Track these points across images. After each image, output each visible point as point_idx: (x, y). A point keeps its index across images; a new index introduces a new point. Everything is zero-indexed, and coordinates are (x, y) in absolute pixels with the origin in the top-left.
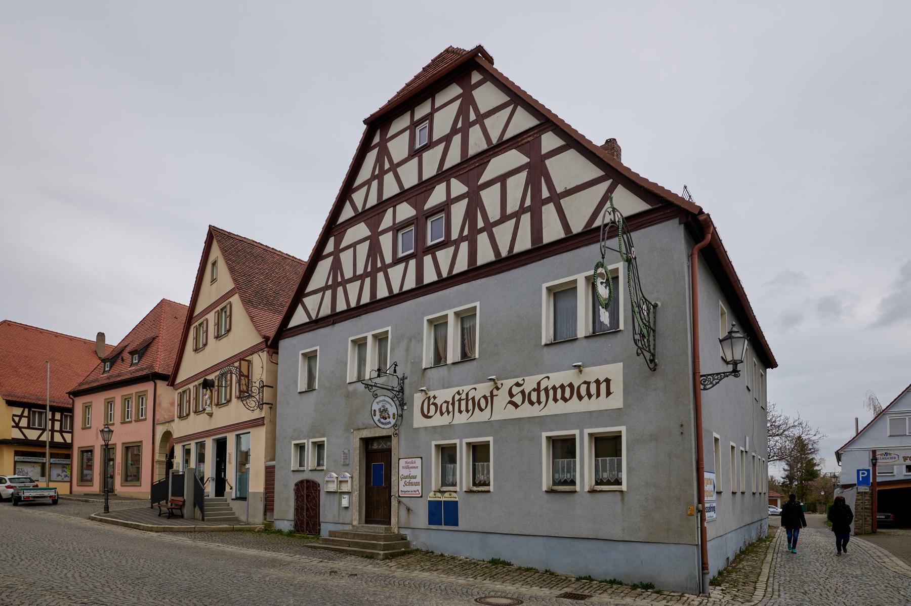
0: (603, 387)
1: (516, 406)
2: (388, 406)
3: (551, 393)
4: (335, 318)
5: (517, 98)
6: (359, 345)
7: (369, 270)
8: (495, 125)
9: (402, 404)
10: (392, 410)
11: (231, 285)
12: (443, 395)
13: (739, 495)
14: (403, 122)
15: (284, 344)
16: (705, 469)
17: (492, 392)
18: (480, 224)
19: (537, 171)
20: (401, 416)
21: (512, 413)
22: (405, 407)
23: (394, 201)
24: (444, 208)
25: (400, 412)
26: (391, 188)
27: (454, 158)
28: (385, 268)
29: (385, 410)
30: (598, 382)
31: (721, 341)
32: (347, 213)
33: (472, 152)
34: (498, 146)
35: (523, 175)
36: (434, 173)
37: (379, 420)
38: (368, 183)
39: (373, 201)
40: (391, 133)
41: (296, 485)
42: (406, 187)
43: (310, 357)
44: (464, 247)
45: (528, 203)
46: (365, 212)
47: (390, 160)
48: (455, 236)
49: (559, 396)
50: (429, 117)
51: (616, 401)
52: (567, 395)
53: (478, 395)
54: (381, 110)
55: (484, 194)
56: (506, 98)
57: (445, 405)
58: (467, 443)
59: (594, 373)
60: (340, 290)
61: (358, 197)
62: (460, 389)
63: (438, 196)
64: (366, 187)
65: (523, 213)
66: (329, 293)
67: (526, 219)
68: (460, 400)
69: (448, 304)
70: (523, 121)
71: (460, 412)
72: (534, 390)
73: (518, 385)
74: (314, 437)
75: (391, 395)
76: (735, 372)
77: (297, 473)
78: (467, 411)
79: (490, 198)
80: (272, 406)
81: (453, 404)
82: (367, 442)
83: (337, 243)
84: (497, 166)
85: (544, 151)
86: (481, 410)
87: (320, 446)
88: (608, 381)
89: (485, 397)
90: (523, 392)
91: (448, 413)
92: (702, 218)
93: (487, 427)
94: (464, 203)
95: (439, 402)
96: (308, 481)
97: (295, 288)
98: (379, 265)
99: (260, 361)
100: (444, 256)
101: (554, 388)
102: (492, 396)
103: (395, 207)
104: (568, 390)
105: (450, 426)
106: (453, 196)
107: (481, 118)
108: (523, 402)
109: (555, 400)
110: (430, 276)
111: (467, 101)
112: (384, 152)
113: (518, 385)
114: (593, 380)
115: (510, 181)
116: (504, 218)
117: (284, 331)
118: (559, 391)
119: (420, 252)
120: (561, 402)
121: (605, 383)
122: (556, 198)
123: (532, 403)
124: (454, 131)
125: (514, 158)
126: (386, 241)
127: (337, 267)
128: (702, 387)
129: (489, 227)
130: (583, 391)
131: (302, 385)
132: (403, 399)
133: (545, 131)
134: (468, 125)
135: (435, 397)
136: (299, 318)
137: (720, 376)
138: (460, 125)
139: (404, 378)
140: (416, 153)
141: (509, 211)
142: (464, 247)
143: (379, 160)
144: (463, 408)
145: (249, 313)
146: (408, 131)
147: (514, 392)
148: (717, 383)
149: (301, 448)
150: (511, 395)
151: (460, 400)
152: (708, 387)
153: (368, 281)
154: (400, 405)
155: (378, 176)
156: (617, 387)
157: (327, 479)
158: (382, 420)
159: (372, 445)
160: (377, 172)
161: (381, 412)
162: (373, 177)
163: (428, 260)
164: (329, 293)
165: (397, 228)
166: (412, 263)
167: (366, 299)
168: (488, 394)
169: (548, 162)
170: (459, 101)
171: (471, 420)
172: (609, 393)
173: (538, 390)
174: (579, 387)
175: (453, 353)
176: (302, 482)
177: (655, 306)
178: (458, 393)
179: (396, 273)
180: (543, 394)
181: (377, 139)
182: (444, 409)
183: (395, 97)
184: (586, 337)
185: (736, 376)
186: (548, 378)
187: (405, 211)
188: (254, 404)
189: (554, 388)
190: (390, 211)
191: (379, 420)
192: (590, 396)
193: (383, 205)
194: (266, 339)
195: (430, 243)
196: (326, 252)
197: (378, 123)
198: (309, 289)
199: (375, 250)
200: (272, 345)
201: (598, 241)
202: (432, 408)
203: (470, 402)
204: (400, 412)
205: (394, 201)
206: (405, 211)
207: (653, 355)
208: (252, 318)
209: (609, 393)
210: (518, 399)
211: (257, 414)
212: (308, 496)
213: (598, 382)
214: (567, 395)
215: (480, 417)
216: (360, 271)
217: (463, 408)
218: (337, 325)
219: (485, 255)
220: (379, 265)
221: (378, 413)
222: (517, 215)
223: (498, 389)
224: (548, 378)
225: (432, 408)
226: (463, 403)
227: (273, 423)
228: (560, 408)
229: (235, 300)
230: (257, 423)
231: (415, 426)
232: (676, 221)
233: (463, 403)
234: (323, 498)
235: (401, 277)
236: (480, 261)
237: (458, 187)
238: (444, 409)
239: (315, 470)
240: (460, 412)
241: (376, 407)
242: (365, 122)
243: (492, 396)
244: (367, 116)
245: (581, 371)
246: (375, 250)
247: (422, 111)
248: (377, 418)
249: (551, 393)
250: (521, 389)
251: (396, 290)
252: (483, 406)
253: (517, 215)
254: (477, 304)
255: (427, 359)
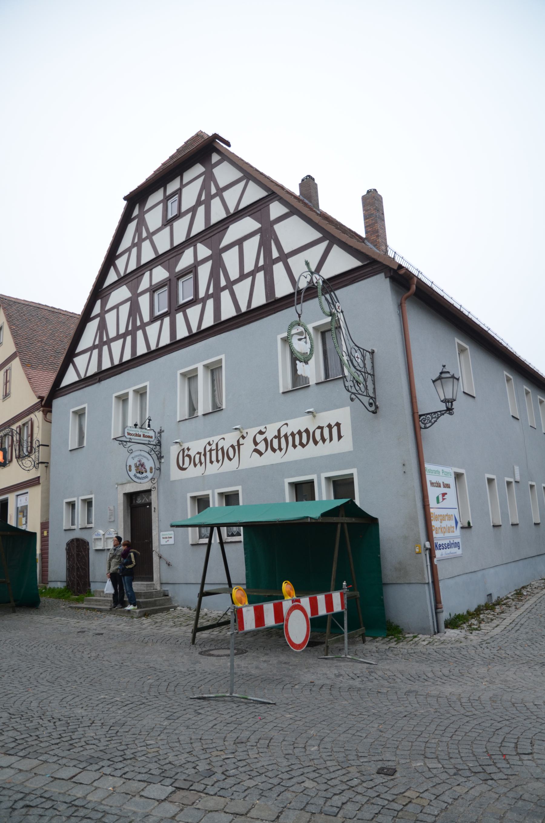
0: (335, 430)
1: (261, 454)
2: (144, 461)
3: (290, 439)
4: (101, 376)
5: (249, 174)
6: (189, 379)
7: (130, 328)
8: (231, 198)
9: (160, 457)
10: (149, 463)
11: (13, 349)
12: (196, 446)
13: (506, 529)
14: (157, 196)
15: (57, 403)
16: (431, 506)
17: (238, 441)
18: (223, 283)
19: (267, 235)
20: (160, 469)
21: (257, 461)
22: (163, 460)
23: (150, 265)
24: (192, 270)
25: (158, 465)
26: (148, 255)
27: (199, 226)
28: (143, 326)
29: (142, 465)
30: (330, 426)
31: (434, 382)
32: (112, 277)
33: (214, 221)
34: (234, 214)
35: (257, 238)
36: (183, 239)
37: (135, 475)
38: (129, 250)
39: (133, 266)
40: (148, 206)
41: (68, 544)
42: (161, 252)
43: (80, 414)
44: (210, 303)
45: (261, 263)
46: (126, 276)
47: (147, 230)
48: (202, 294)
49: (297, 442)
50: (179, 192)
51: (346, 445)
52: (304, 441)
53: (226, 445)
54: (139, 187)
55: (225, 256)
56: (239, 175)
57: (197, 456)
58: (326, 478)
59: (328, 417)
60: (105, 348)
61: (121, 263)
62: (210, 439)
63: (186, 259)
64: (190, 215)
65: (258, 272)
66: (96, 352)
67: (260, 276)
68: (211, 451)
69: (196, 357)
70: (254, 193)
71: (211, 462)
72: (275, 437)
73: (261, 433)
74: (83, 495)
75: (147, 449)
76: (449, 410)
77: (68, 532)
78: (218, 461)
79: (230, 259)
80: (46, 464)
81: (205, 455)
82: (130, 497)
83: (103, 306)
84: (234, 231)
85: (273, 217)
86: (230, 459)
87: (89, 503)
88: (338, 425)
89: (232, 446)
90: (265, 440)
91: (201, 464)
92: (402, 272)
93: (236, 476)
94: (209, 264)
95: (192, 453)
96: (78, 540)
97: (67, 347)
98: (138, 323)
99: (38, 417)
100: (193, 312)
101: (293, 435)
102: (239, 445)
103: (151, 270)
104: (304, 435)
105: (203, 476)
106: (200, 258)
107: (220, 191)
108: (266, 450)
109: (294, 446)
110: (182, 333)
111: (209, 177)
112: (142, 223)
113: (261, 433)
114: (325, 424)
115: (246, 244)
116: (243, 277)
117: (56, 391)
118: (297, 437)
119: (173, 310)
120: (299, 447)
121: (336, 428)
122: (284, 257)
123: (274, 450)
124: (199, 203)
125: (248, 224)
126: (144, 301)
127: (102, 327)
128: (423, 426)
129: (230, 285)
130: (318, 437)
131: (73, 443)
132: (160, 452)
133: (272, 201)
134: (210, 197)
135: (188, 449)
136: (70, 377)
137: (438, 414)
138: (203, 198)
139: (161, 432)
140: (168, 222)
141: (247, 270)
142: (210, 303)
143: (138, 230)
144: (214, 458)
145: (27, 375)
146: (161, 204)
147: (258, 440)
148: (435, 421)
149: (72, 505)
150: (256, 443)
151: (211, 451)
152: (428, 425)
153: (129, 338)
154: (158, 458)
155: (137, 244)
156: (346, 430)
157: (94, 537)
158: (138, 475)
159: (136, 500)
160: (136, 241)
161: (136, 466)
162: (133, 245)
163: (180, 317)
164: (96, 352)
165: (153, 290)
166: (167, 320)
167: (127, 356)
168: (235, 444)
169: (276, 227)
170: (202, 179)
171: (222, 470)
172: (340, 437)
173: (278, 437)
174: (314, 432)
175: (204, 405)
176: (72, 541)
177: (372, 353)
178: (209, 444)
179: (152, 330)
180: (283, 440)
181: (136, 212)
182: (197, 461)
183: (159, 168)
184: (317, 384)
185: (451, 414)
186: (287, 424)
187: (160, 274)
188: (29, 464)
189: (293, 435)
190: (147, 274)
191: (135, 475)
192: (324, 440)
193: (141, 269)
194: (41, 398)
195: (181, 301)
196: (94, 314)
197: (137, 199)
198: (79, 349)
199: (135, 310)
200: (46, 405)
201: (294, 305)
202: (187, 459)
203: (220, 452)
204: (158, 465)
205: (150, 265)
206: (160, 274)
207: (374, 398)
208: (29, 379)
209: (340, 437)
210: (262, 447)
211: (33, 474)
212: (78, 555)
213: (330, 426)
214: (304, 441)
215: (229, 466)
216: (122, 330)
217: (214, 458)
218: (103, 382)
219: (228, 312)
220: (138, 323)
221: (133, 468)
222: (253, 274)
223: (243, 437)
224: (287, 424)
225: (187, 459)
226: (214, 453)
227: (48, 479)
228: (296, 454)
229: (16, 363)
230: (34, 482)
231: (172, 478)
232: (382, 275)
233: (214, 453)
234: (92, 556)
235: (157, 335)
236: (179, 337)
237: (203, 251)
238: (197, 461)
239: (86, 528)
240: (211, 462)
241: (132, 462)
242: (125, 198)
243: (239, 445)
244: (127, 193)
245: (314, 416)
246: (135, 310)
247: (173, 186)
248: (132, 474)
249: (290, 439)
250: (263, 437)
251: (153, 347)
252: (231, 455)
253: (253, 274)
254: (223, 357)
255: (181, 409)
